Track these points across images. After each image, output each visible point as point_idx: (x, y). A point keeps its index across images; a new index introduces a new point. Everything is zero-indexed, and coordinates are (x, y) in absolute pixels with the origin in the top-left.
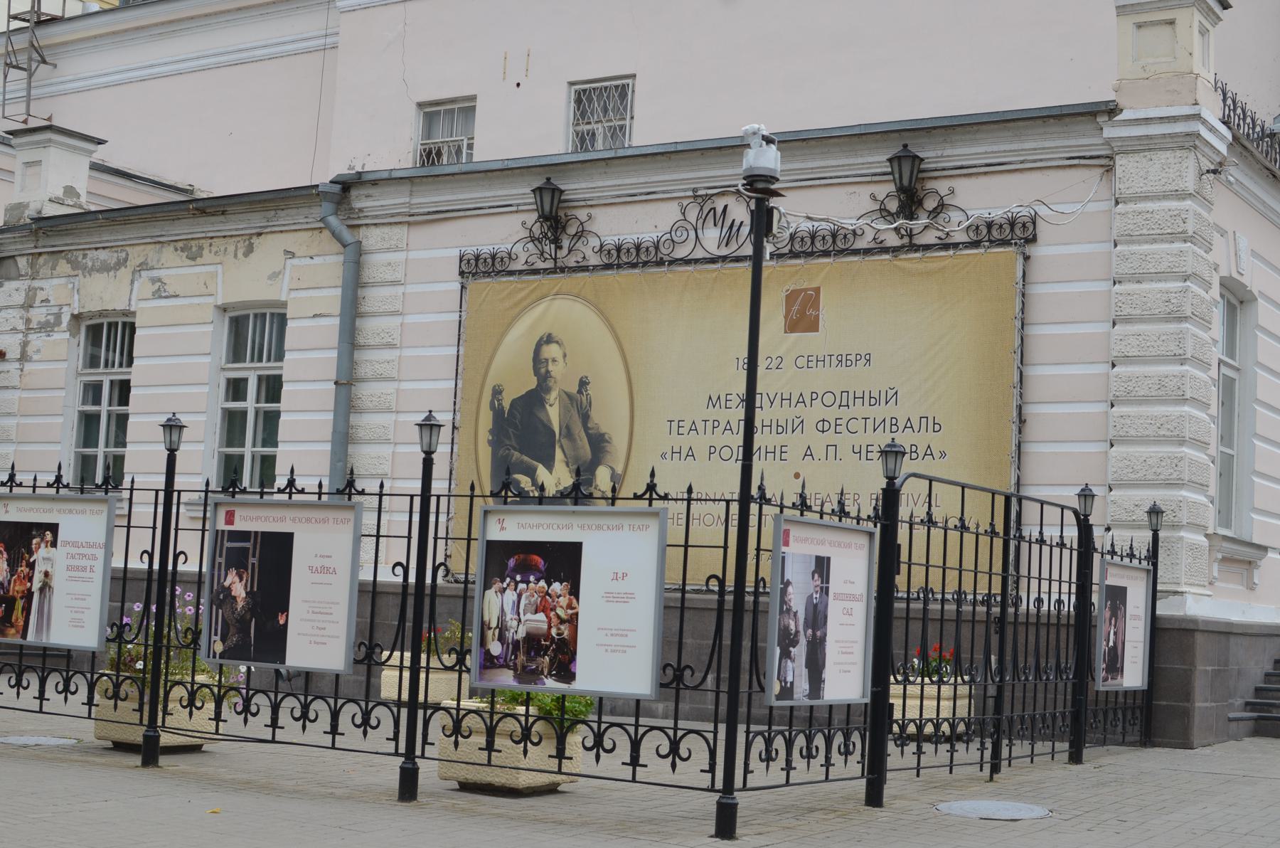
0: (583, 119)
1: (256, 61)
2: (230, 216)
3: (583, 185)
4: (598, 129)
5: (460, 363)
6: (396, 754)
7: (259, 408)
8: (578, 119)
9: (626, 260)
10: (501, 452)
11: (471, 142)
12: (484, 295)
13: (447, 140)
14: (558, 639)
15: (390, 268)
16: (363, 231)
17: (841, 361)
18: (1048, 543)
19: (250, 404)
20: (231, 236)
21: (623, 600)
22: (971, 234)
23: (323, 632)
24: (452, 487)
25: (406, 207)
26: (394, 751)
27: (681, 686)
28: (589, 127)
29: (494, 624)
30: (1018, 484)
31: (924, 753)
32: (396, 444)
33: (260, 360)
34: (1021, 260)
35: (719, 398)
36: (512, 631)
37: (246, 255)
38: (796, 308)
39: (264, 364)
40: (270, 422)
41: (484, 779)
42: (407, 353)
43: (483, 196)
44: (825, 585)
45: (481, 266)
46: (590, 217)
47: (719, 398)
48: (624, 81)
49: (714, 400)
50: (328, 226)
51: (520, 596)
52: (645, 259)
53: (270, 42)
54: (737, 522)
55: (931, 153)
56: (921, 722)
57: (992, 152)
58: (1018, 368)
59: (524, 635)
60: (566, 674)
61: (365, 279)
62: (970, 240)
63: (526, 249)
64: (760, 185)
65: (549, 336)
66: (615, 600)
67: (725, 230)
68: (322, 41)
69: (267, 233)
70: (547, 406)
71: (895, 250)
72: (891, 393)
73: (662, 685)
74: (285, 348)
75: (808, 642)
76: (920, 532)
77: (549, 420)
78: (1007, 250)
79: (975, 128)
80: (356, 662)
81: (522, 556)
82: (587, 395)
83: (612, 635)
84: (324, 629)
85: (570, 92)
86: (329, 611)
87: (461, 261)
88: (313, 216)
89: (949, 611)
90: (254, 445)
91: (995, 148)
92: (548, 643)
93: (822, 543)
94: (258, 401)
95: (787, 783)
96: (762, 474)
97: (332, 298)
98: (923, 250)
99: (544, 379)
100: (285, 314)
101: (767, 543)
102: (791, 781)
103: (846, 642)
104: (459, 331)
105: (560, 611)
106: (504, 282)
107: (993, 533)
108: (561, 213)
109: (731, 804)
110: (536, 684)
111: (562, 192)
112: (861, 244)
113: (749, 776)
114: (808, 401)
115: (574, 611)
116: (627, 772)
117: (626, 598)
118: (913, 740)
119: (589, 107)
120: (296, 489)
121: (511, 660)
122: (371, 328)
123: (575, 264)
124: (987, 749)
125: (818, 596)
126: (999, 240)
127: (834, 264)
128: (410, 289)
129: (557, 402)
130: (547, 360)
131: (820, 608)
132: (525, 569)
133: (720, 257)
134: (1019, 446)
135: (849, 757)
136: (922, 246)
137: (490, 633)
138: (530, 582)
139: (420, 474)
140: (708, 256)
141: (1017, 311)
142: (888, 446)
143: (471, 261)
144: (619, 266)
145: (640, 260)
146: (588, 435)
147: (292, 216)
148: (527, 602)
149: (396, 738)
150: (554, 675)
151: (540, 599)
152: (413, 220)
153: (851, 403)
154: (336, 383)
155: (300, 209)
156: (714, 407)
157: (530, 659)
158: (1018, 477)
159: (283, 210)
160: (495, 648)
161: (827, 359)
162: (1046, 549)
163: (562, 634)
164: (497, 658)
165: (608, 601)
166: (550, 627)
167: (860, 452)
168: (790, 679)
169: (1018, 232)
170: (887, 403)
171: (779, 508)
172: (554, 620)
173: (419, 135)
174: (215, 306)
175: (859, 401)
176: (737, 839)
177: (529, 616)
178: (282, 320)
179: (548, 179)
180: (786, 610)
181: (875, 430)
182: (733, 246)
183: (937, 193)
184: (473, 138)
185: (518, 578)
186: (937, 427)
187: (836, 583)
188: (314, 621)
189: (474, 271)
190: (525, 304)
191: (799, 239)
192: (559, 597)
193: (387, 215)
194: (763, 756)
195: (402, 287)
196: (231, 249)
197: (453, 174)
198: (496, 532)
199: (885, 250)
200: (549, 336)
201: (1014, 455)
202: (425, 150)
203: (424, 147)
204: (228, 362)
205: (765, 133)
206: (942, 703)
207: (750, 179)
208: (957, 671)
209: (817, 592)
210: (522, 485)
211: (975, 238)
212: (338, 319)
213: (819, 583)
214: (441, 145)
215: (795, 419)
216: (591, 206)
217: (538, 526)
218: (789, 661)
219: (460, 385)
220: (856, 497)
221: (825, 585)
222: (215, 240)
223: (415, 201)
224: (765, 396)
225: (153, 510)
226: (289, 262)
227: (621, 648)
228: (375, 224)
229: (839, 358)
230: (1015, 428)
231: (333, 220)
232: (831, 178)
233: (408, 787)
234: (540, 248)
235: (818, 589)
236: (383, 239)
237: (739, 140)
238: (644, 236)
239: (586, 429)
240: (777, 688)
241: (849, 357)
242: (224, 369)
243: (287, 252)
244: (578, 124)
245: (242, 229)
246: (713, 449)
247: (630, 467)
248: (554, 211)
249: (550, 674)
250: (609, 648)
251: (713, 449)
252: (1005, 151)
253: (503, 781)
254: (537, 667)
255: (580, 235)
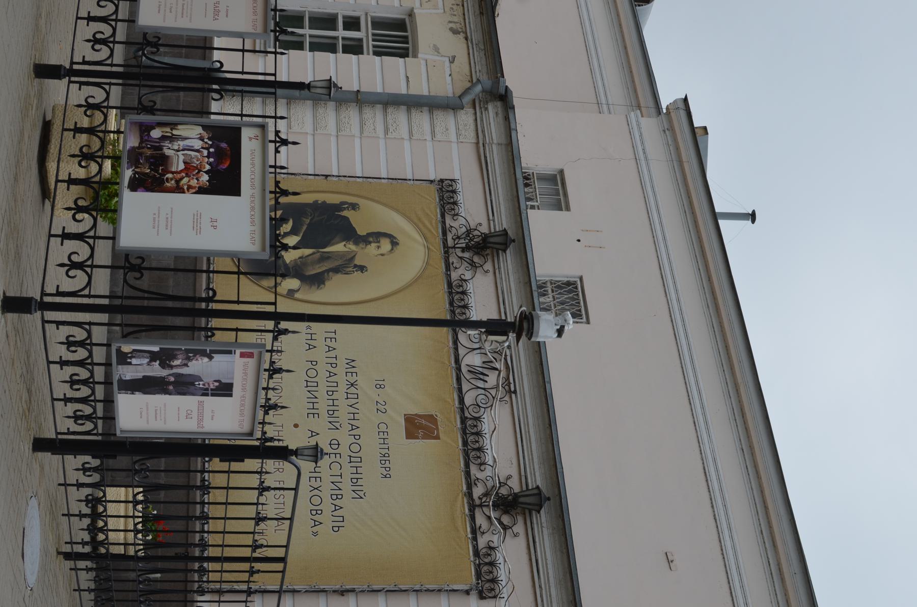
0: (555, 287)
1: (589, 60)
2: (479, 18)
3: (510, 267)
4: (549, 298)
5: (375, 180)
6: (72, 63)
7: (338, 40)
8: (555, 284)
9: (455, 298)
10: (309, 210)
11: (536, 208)
12: (426, 196)
13: (537, 190)
14: (164, 179)
15: (444, 130)
16: (471, 111)
17: (384, 457)
18: (249, 599)
19: (341, 33)
20: (465, 19)
21: (195, 226)
22: (484, 551)
23: (168, 10)
24: (282, 175)
25: (489, 141)
26: (74, 61)
27: (126, 270)
28: (550, 291)
29: (175, 132)
30: (294, 591)
31: (81, 520)
32: (314, 135)
33: (373, 40)
34: (466, 588)
35: (354, 367)
36: (170, 145)
37: (451, 29)
38: (424, 422)
39: (371, 43)
40: (330, 47)
41: (54, 137)
42: (382, 143)
43: (500, 195)
44: (210, 392)
45: (447, 194)
46: (487, 272)
47: (354, 367)
48: (584, 316)
49: (352, 364)
50: (473, 85)
51: (197, 151)
52: (456, 312)
53: (603, 69)
54: (260, 342)
55: (544, 517)
56: (94, 418)
57: (547, 564)
58: (384, 589)
59: (166, 154)
60: (135, 185)
61: (435, 113)
62: (479, 549)
63: (461, 226)
64: (525, 325)
65: (397, 244)
66: (195, 220)
67: (480, 369)
68: (604, 101)
69: (467, 44)
70: (344, 243)
71: (470, 494)
72: (361, 494)
73: (127, 256)
74: (383, 57)
75: (164, 378)
76: (254, 481)
77: (333, 244)
78: (473, 577)
79: (565, 551)
80: (145, 34)
81: (229, 152)
82: (353, 271)
83: (167, 218)
84: (171, 12)
85: (575, 278)
86: (185, 16)
87: (451, 180)
88: (481, 76)
89: (194, 537)
90: (311, 36)
91: (550, 566)
92: (160, 171)
93: (244, 389)
94: (343, 39)
95: (49, 362)
96: (297, 332)
97: (421, 88)
98: (470, 515)
99: (365, 240)
100: (408, 57)
101: (244, 337)
102: (51, 366)
103: (165, 413)
104: (399, 179)
105: (185, 180)
106: (436, 211)
107: (255, 546)
108: (488, 251)
109: (31, 308)
110: (128, 163)
111: (505, 251)
112: (474, 470)
113: (54, 326)
114: (353, 432)
115: (186, 190)
116: (57, 230)
117: (197, 226)
118: (92, 511)
119: (565, 291)
120: (279, 146)
121: (147, 144)
122: (399, 117)
123: (451, 261)
124: (83, 547)
125: (201, 386)
126: (481, 571)
127: (457, 450)
128: (429, 144)
129: (347, 250)
130: (379, 242)
131: (192, 388)
132: (219, 155)
133: (460, 366)
134: (323, 591)
135: (64, 347)
136: (474, 514)
137: (168, 130)
138: (208, 158)
139: (292, 80)
140: (461, 358)
141: (427, 586)
142: (322, 450)
143: (451, 188)
144: (450, 293)
145: (455, 308)
146: (323, 272)
147: (481, 61)
148: (193, 156)
149: (84, 62)
150: (135, 176)
151: (195, 165)
152: (480, 146)
153: (353, 464)
154: (358, 91)
155: (486, 66)
156: (347, 364)
157: (147, 159)
158: (300, 591)
159: (485, 54)
160: (156, 133)
161: (386, 446)
162: (245, 576)
163: (168, 182)
164: (149, 135)
165: (194, 215)
166: (173, 173)
167: (315, 472)
168: (134, 361)
169: (487, 585)
170: (353, 491)
171: (270, 349)
172: (179, 176)
173: (540, 171)
174: (413, 8)
175: (354, 470)
176: (2, 314)
177: (182, 158)
178: (404, 54)
179: (514, 241)
180: (191, 355)
181: (332, 483)
182: (468, 376)
183: (514, 524)
184: (539, 209)
185: (212, 150)
186: (336, 529)
187: (211, 402)
188: (177, 5)
189: (444, 190)
190: (421, 225)
191: (475, 424)
192: (197, 179)
193: (483, 128)
194: (78, 413)
195: (431, 139)
196: (455, 19)
197: (515, 173)
198: (247, 135)
199: (470, 487)
200: (397, 244)
201: (316, 587)
202: (529, 175)
203: (531, 175)
204: (372, 18)
205: (566, 328)
206: (122, 533)
207: (529, 316)
208: (147, 545)
209: (204, 385)
210: (284, 225)
211: (481, 553)
212: (406, 93)
213: (212, 386)
214: (533, 186)
215: (339, 424)
216: (495, 273)
217: (253, 164)
218: (148, 360)
219: (358, 180)
220: (281, 470)
221: (210, 392)
222: (461, 7)
223: (494, 147)
224: (356, 401)
225: (260, 72)
226: (447, 59)
227: (156, 225)
228: (476, 120)
229: (387, 455)
230: (337, 587)
231: (479, 88)
232: (522, 446)
233: (45, 71)
234: (463, 236)
235: (207, 386)
236: (466, 125)
237: (548, 380)
238: (474, 311)
239: (328, 271)
240: (126, 348)
241: (387, 462)
242: (366, 14)
243: (454, 57)
244: (551, 283)
245: (470, 27)
246: (315, 363)
247: (299, 303)
248: (491, 245)
249: (135, 173)
250: (156, 216)
251: (315, 363)
252: (548, 573)
253: (51, 151)
254: (141, 164)
255: (473, 265)
